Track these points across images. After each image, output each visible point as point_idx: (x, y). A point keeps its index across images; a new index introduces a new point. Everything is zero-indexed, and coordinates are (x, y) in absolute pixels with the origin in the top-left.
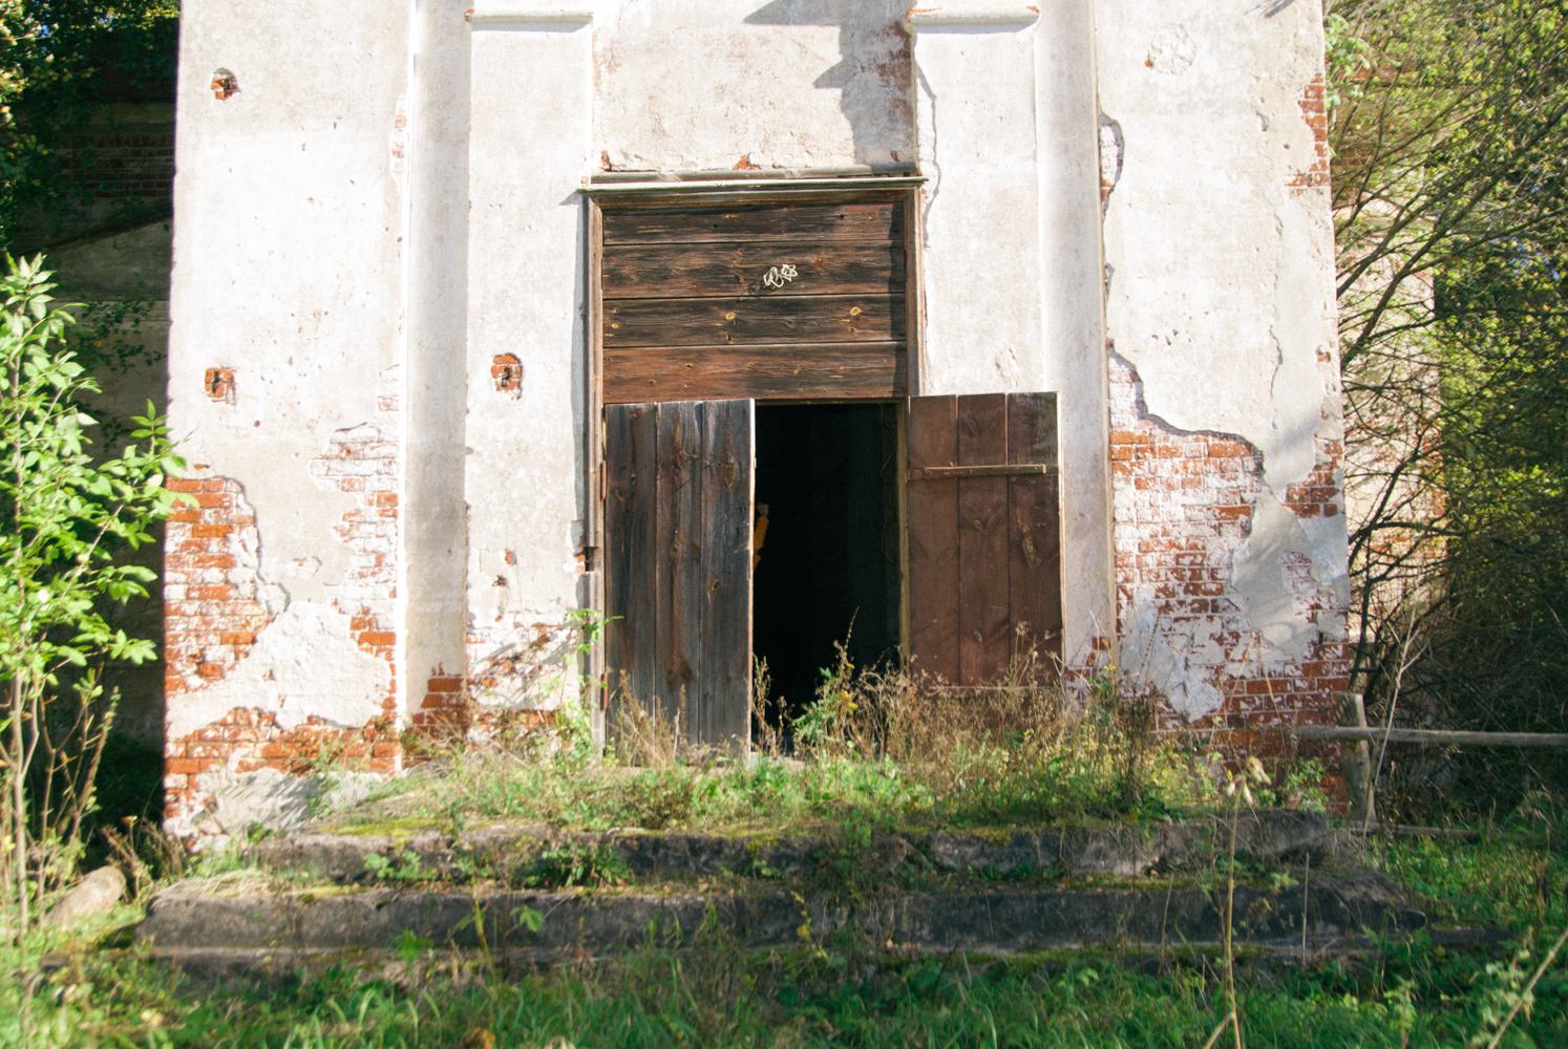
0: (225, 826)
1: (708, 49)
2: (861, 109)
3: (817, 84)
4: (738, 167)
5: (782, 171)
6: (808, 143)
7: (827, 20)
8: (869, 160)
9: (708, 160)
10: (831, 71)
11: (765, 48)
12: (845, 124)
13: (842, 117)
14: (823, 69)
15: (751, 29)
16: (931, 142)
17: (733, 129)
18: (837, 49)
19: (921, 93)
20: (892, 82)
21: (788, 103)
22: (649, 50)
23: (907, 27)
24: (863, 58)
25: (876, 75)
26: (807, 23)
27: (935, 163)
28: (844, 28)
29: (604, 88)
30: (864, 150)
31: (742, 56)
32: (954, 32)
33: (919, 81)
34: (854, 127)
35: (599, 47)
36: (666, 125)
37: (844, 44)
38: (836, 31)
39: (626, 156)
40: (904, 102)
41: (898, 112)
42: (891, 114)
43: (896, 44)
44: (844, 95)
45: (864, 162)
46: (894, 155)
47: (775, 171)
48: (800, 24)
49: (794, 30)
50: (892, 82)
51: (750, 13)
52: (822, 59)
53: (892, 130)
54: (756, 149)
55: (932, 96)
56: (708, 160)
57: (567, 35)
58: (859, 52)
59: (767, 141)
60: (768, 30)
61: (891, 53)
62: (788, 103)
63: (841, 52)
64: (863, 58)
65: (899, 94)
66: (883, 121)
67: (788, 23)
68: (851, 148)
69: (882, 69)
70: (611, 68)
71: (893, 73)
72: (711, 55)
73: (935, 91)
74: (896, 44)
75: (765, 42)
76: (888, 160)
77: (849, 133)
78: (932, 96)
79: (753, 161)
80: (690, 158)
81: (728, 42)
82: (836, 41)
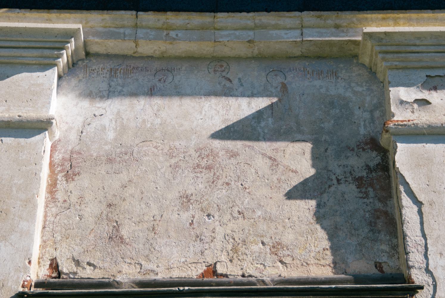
0: (440, 255)
1: (173, 161)
2: (338, 219)
3: (290, 195)
4: (203, 275)
5: (253, 279)
6: (281, 253)
7: (299, 136)
8: (350, 270)
9: (169, 269)
10: (305, 183)
11: (233, 161)
12: (322, 234)
13: (318, 227)
14: (296, 181)
15: (217, 144)
16: (422, 249)
17: (199, 238)
18: (310, 162)
19: (406, 200)
20: (371, 194)
21: (259, 213)
22: (110, 161)
23: (383, 141)
24: (339, 171)
25: (353, 187)
26: (277, 140)
27: (428, 271)
28: (316, 143)
29: (60, 196)
30: (344, 261)
31: (209, 168)
32: (436, 142)
33: (402, 188)
34: (331, 237)
35: (58, 157)
36: (124, 232)
37: (316, 158)
38: (308, 147)
39: (77, 263)
40: (386, 213)
41: (380, 225)
42: (372, 225)
43: (374, 158)
44: (318, 206)
45: (345, 273)
46: (378, 266)
47: (245, 280)
48: (270, 139)
49: (264, 146)
50: (371, 194)
51: (218, 129)
52: (296, 172)
53: (375, 240)
54: (224, 257)
55: (419, 203)
56: (169, 269)
57: (22, 140)
58: (334, 165)
59: (235, 250)
60: (238, 145)
61: (367, 166)
62: (259, 213)
63: (313, 166)
64: (339, 171)
65: (379, 205)
66: (365, 231)
67: (257, 139)
68: (329, 258)
69: (359, 182)
70: (69, 176)
71: (371, 185)
72: (176, 166)
73: (421, 197)
74: (374, 158)
75: (234, 155)
76: (374, 271)
77: (326, 244)
78: (419, 203)
79: (220, 269)
80: (151, 266)
81: (195, 155)
82: (308, 155)
